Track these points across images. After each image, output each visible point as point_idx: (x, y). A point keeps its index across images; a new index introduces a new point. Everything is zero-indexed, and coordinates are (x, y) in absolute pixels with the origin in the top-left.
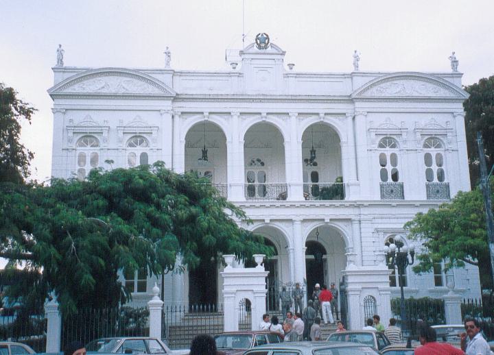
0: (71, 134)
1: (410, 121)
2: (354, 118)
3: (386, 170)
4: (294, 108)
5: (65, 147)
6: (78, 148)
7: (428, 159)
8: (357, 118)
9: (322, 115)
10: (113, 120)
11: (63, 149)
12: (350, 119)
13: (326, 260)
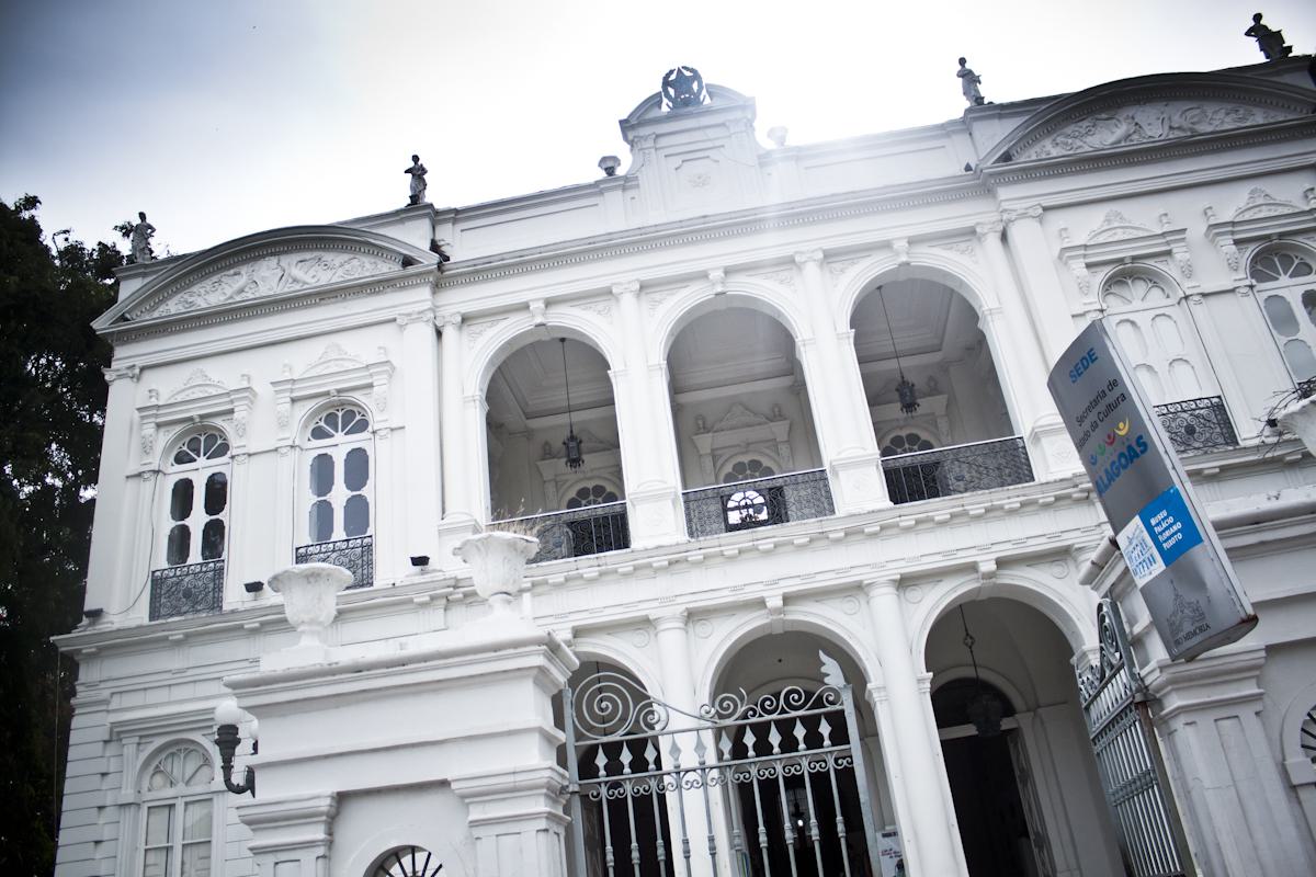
0: (149, 430)
1: (1189, 212)
2: (1004, 237)
3: (328, 504)
4: (809, 240)
5: (133, 468)
6: (171, 470)
7: (322, 471)
8: (1013, 232)
9: (536, 306)
10: (262, 370)
11: (128, 477)
12: (993, 240)
13: (1014, 733)
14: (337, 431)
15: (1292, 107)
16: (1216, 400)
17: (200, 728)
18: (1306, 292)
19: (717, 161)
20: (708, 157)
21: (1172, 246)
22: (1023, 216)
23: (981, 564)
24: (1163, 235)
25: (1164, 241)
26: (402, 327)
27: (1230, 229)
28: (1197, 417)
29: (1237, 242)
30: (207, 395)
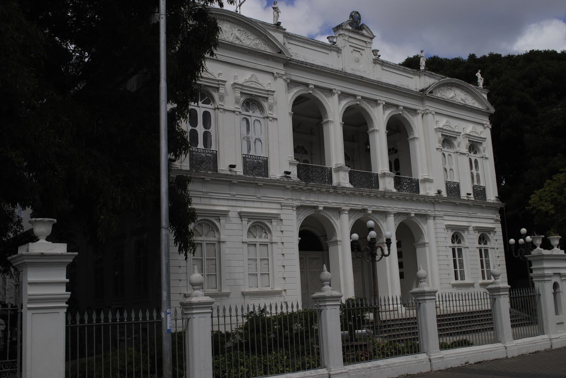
14: (201, 101)
15: (275, 50)
16: (215, 152)
17: (248, 216)
18: (205, 111)
19: (362, 55)
20: (359, 52)
21: (269, 96)
22: (430, 113)
23: (193, 199)
24: (268, 91)
25: (267, 93)
26: (275, 78)
27: (241, 87)
28: (207, 156)
29: (241, 93)
30: (257, 87)
